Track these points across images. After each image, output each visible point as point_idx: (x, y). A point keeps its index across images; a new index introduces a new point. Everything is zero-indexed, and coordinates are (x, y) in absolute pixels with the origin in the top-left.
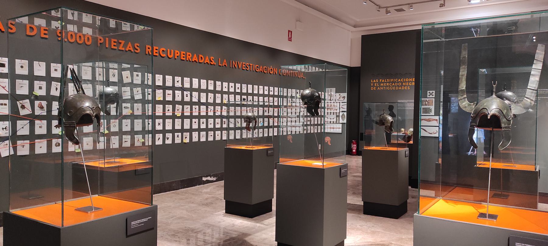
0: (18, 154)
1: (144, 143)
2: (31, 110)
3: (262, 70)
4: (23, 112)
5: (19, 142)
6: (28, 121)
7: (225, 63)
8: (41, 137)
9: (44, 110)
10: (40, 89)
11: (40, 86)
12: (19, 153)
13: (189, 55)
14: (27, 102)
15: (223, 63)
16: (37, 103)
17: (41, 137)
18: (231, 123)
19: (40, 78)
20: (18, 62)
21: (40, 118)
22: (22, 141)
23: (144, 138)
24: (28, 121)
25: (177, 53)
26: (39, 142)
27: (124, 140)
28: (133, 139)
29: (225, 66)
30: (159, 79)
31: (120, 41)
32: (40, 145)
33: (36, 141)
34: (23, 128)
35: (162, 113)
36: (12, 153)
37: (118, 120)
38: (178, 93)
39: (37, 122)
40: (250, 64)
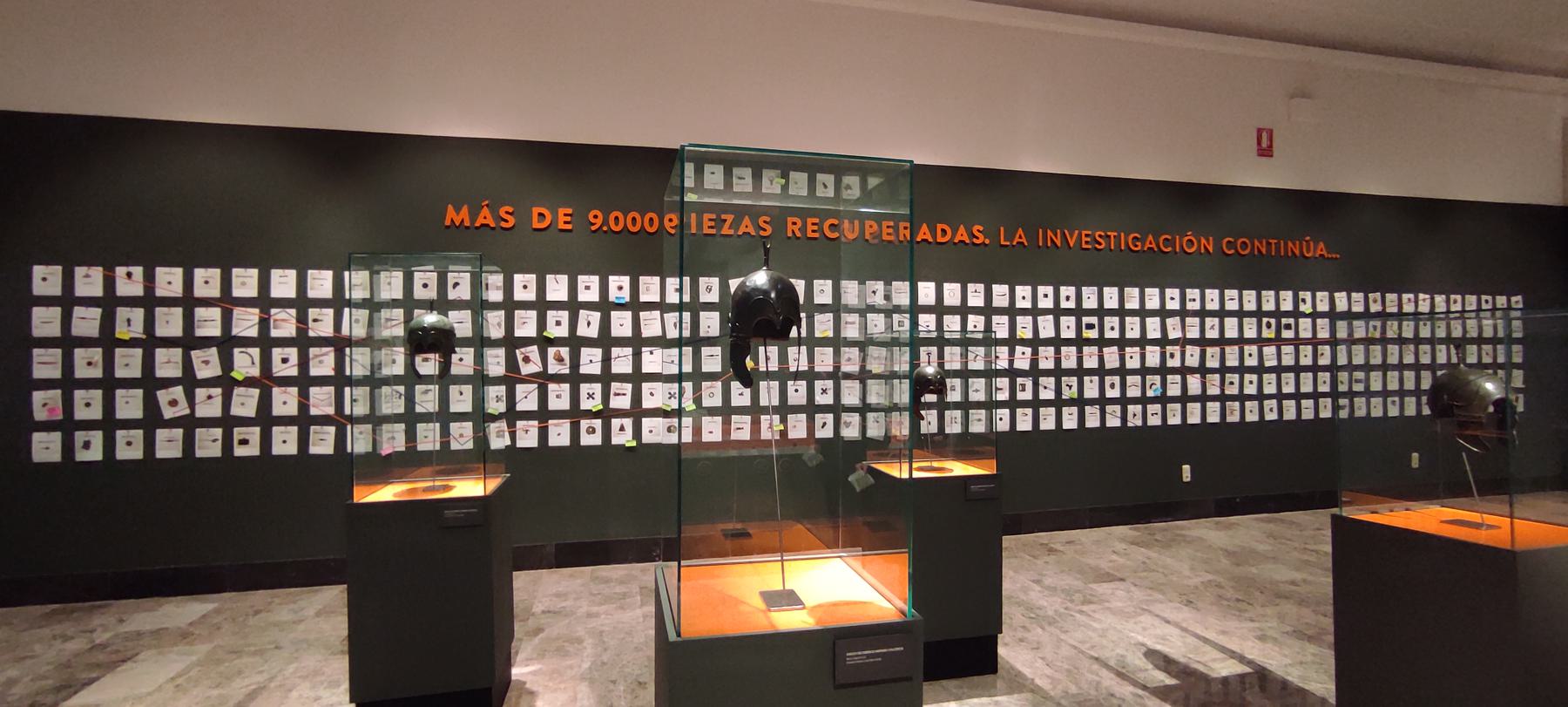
0: (518, 446)
1: (784, 433)
2: (541, 366)
3: (1154, 246)
4: (526, 369)
5: (520, 424)
6: (536, 386)
7: (1020, 237)
8: (559, 415)
9: (565, 365)
10: (557, 326)
11: (558, 319)
12: (520, 444)
13: (794, 223)
14: (533, 351)
15: (1014, 236)
16: (551, 351)
17: (559, 415)
18: (1045, 388)
19: (557, 305)
20: (518, 278)
21: (558, 378)
22: (525, 422)
23: (784, 421)
24: (536, 386)
25: (871, 226)
26: (556, 425)
27: (733, 426)
28: (756, 424)
29: (1021, 246)
30: (927, 292)
31: (723, 217)
32: (559, 430)
33: (550, 422)
34: (526, 397)
35: (1007, 361)
36: (508, 442)
37: (720, 383)
38: (1193, 322)
39: (552, 387)
40: (1109, 233)
